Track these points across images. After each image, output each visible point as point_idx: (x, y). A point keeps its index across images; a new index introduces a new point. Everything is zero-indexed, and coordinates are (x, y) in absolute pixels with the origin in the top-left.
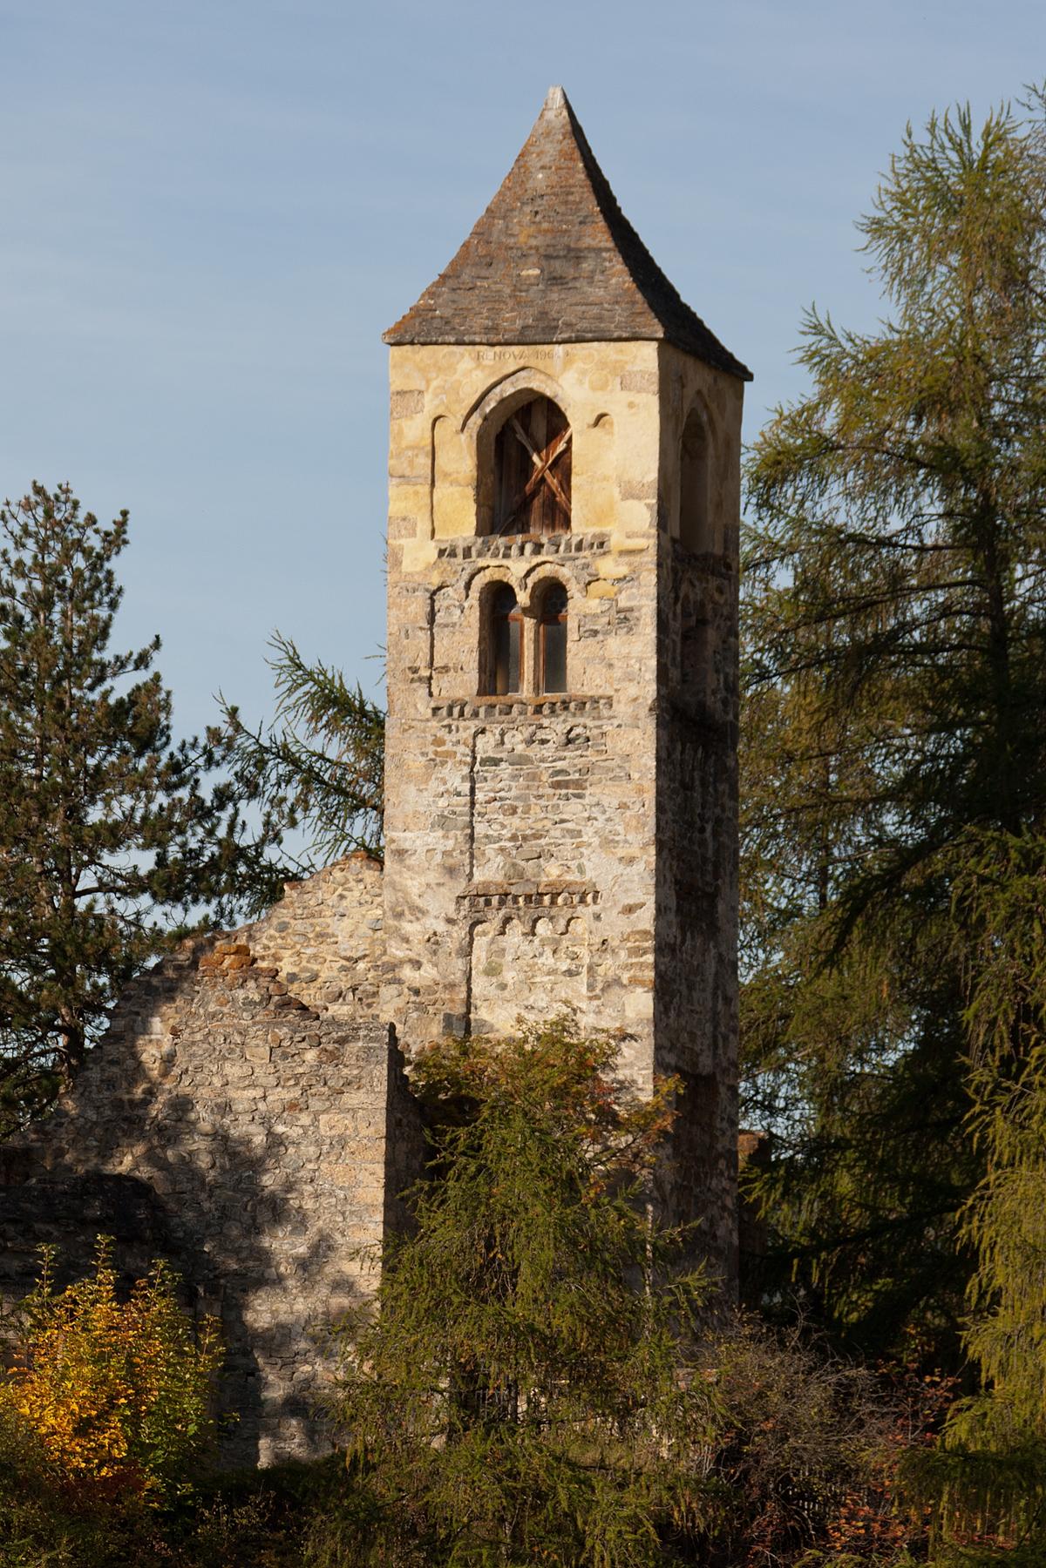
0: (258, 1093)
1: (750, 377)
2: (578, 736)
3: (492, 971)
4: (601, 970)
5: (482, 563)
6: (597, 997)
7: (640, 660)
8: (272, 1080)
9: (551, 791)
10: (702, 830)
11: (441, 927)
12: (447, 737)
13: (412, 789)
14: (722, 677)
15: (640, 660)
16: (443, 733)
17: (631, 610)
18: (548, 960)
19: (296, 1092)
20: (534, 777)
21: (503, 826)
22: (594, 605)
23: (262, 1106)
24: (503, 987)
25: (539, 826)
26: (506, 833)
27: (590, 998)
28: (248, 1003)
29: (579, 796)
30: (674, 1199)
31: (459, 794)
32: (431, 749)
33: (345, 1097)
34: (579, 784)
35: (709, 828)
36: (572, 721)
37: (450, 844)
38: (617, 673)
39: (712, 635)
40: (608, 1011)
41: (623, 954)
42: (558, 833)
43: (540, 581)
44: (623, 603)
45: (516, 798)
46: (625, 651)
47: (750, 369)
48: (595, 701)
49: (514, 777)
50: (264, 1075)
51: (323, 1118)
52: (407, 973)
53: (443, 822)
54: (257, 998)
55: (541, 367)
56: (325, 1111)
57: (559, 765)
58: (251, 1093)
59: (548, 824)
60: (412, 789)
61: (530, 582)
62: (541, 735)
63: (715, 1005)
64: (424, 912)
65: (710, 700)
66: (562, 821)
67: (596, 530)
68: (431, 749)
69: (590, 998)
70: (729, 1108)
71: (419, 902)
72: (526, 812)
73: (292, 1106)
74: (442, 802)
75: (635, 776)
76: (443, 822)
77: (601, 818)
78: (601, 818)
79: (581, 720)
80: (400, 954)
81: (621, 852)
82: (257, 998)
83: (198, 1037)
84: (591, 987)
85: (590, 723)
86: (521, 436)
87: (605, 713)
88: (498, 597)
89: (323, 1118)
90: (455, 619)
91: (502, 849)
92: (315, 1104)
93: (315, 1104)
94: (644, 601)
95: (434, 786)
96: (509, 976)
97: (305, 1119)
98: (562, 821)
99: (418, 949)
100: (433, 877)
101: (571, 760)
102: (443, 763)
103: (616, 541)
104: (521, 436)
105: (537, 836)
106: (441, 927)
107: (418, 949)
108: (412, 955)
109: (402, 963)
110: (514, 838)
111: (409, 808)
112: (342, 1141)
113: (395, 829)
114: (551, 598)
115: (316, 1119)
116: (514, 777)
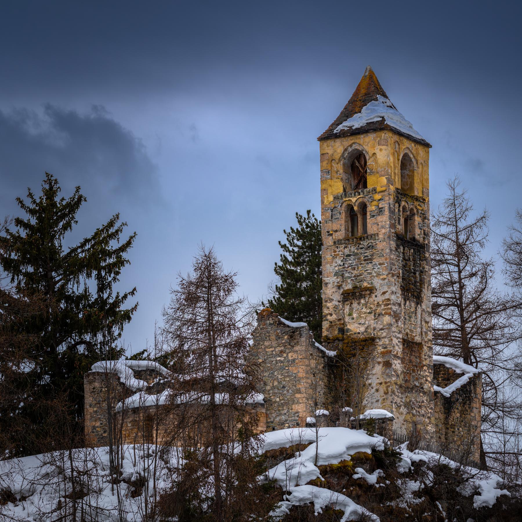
0: (273, 349)
1: (431, 147)
2: (370, 246)
3: (350, 315)
4: (377, 311)
5: (344, 199)
6: (376, 319)
7: (385, 222)
8: (277, 345)
9: (363, 262)
10: (415, 273)
11: (337, 303)
12: (337, 250)
13: (329, 265)
14: (422, 231)
15: (385, 222)
16: (336, 249)
17: (382, 208)
18: (364, 310)
19: (283, 348)
20: (359, 259)
21: (352, 273)
22: (374, 208)
23: (274, 353)
24: (353, 319)
25: (361, 272)
26: (353, 275)
27: (375, 319)
28: (270, 324)
29: (371, 263)
30: (402, 376)
31: (340, 266)
32: (333, 254)
33: (294, 348)
34: (371, 259)
35: (418, 273)
36: (369, 242)
37: (339, 280)
38: (380, 226)
39: (417, 219)
40: (379, 322)
41: (383, 306)
42: (366, 274)
43: (360, 203)
44: (380, 206)
45: (355, 265)
46: (381, 220)
47: (428, 141)
48: (375, 235)
49: (354, 259)
50: (274, 344)
51: (290, 355)
52: (329, 317)
53: (336, 274)
54: (272, 322)
55: (358, 142)
56: (289, 353)
57: (366, 254)
58: (271, 349)
59: (363, 271)
60: (329, 265)
61: (357, 204)
62: (361, 246)
63: (421, 323)
64: (333, 300)
65: (417, 237)
66: (367, 270)
67: (373, 187)
68: (333, 254)
69: (375, 319)
70: (428, 353)
71: (331, 297)
72: (358, 269)
73: (281, 352)
74: (337, 268)
75: (385, 255)
76: (336, 274)
77: (376, 268)
78: (376, 268)
79: (371, 241)
80: (327, 312)
81: (381, 277)
82: (272, 322)
83: (258, 335)
84: (375, 316)
85: (373, 242)
86: (357, 164)
87: (377, 238)
88: (350, 208)
89: (290, 355)
90: (338, 216)
91: (352, 280)
92: (287, 351)
93: (287, 351)
94: (386, 205)
95: (334, 264)
96: (355, 315)
97: (285, 355)
98: (367, 270)
99: (331, 310)
100: (334, 290)
101: (368, 253)
102: (336, 257)
103: (379, 189)
104: (357, 164)
105: (361, 275)
106: (337, 303)
107: (331, 310)
108: (330, 312)
109: (327, 315)
110: (355, 276)
111: (328, 271)
112: (294, 360)
113: (325, 277)
114: (363, 207)
115: (287, 355)
116: (354, 259)
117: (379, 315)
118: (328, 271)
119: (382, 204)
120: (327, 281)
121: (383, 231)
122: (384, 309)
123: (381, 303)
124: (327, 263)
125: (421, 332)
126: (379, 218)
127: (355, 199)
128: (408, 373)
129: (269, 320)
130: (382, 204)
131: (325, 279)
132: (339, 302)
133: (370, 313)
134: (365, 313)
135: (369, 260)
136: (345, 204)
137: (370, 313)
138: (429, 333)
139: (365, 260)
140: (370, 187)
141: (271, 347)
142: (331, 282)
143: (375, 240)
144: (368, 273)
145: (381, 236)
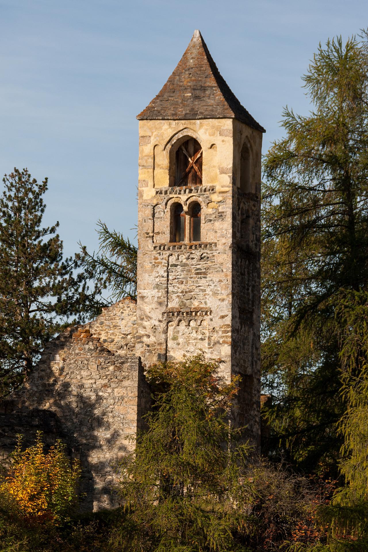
0: (93, 381)
2: (205, 256)
3: (175, 338)
4: (213, 338)
5: (171, 196)
6: (211, 348)
7: (226, 230)
8: (98, 377)
9: (195, 276)
10: (248, 289)
11: (157, 323)
12: (159, 257)
13: (147, 275)
14: (255, 236)
15: (226, 230)
16: (157, 256)
17: (223, 212)
18: (194, 335)
20: (189, 271)
21: (179, 288)
22: (210, 211)
23: (94, 386)
24: (178, 344)
25: (191, 288)
26: (180, 290)
27: (209, 348)
28: (89, 350)
31: (163, 277)
32: (154, 261)
35: (250, 289)
36: (202, 251)
37: (160, 294)
38: (218, 234)
39: (251, 221)
40: (215, 352)
41: (220, 333)
42: (198, 290)
43: (191, 202)
44: (220, 210)
45: (183, 278)
47: (265, 128)
48: (211, 244)
49: (182, 271)
50: (95, 375)
53: (157, 286)
54: (93, 348)
56: (116, 388)
57: (198, 267)
59: (194, 287)
60: (147, 275)
61: (188, 203)
62: (192, 256)
64: (151, 318)
66: (199, 286)
67: (211, 184)
70: (257, 387)
71: (149, 315)
72: (187, 283)
73: (105, 386)
74: (157, 280)
75: (225, 270)
76: (157, 286)
77: (213, 285)
78: (213, 285)
79: (206, 251)
80: (143, 333)
82: (93, 348)
83: (72, 361)
84: (209, 344)
85: (209, 252)
86: (185, 152)
87: (214, 248)
88: (177, 208)
89: (116, 390)
90: (162, 216)
91: (178, 296)
92: (113, 385)
93: (113, 385)
94: (228, 210)
95: (154, 274)
96: (181, 340)
97: (109, 390)
98: (199, 286)
99: (149, 331)
100: (154, 306)
101: (202, 265)
102: (158, 266)
103: (218, 188)
104: (185, 152)
107: (149, 331)
108: (147, 333)
109: (143, 336)
110: (182, 292)
111: (146, 282)
112: (122, 398)
113: (141, 289)
114: (195, 208)
115: (113, 390)
116: (182, 271)
117: (215, 344)
118: (146, 282)
119: (223, 208)
120: (145, 295)
121: (224, 241)
122: (222, 337)
123: (217, 329)
124: (146, 271)
125: (252, 362)
126: (217, 224)
127: (186, 197)
128: (242, 414)
129: (87, 344)
130: (223, 208)
131: (141, 291)
132: (160, 321)
133: (202, 339)
134: (196, 339)
135: (201, 274)
136: (170, 203)
137: (202, 339)
138: (258, 361)
139: (197, 274)
140: (206, 183)
141: (91, 379)
142: (150, 296)
143: (212, 250)
144: (201, 290)
145: (220, 247)
